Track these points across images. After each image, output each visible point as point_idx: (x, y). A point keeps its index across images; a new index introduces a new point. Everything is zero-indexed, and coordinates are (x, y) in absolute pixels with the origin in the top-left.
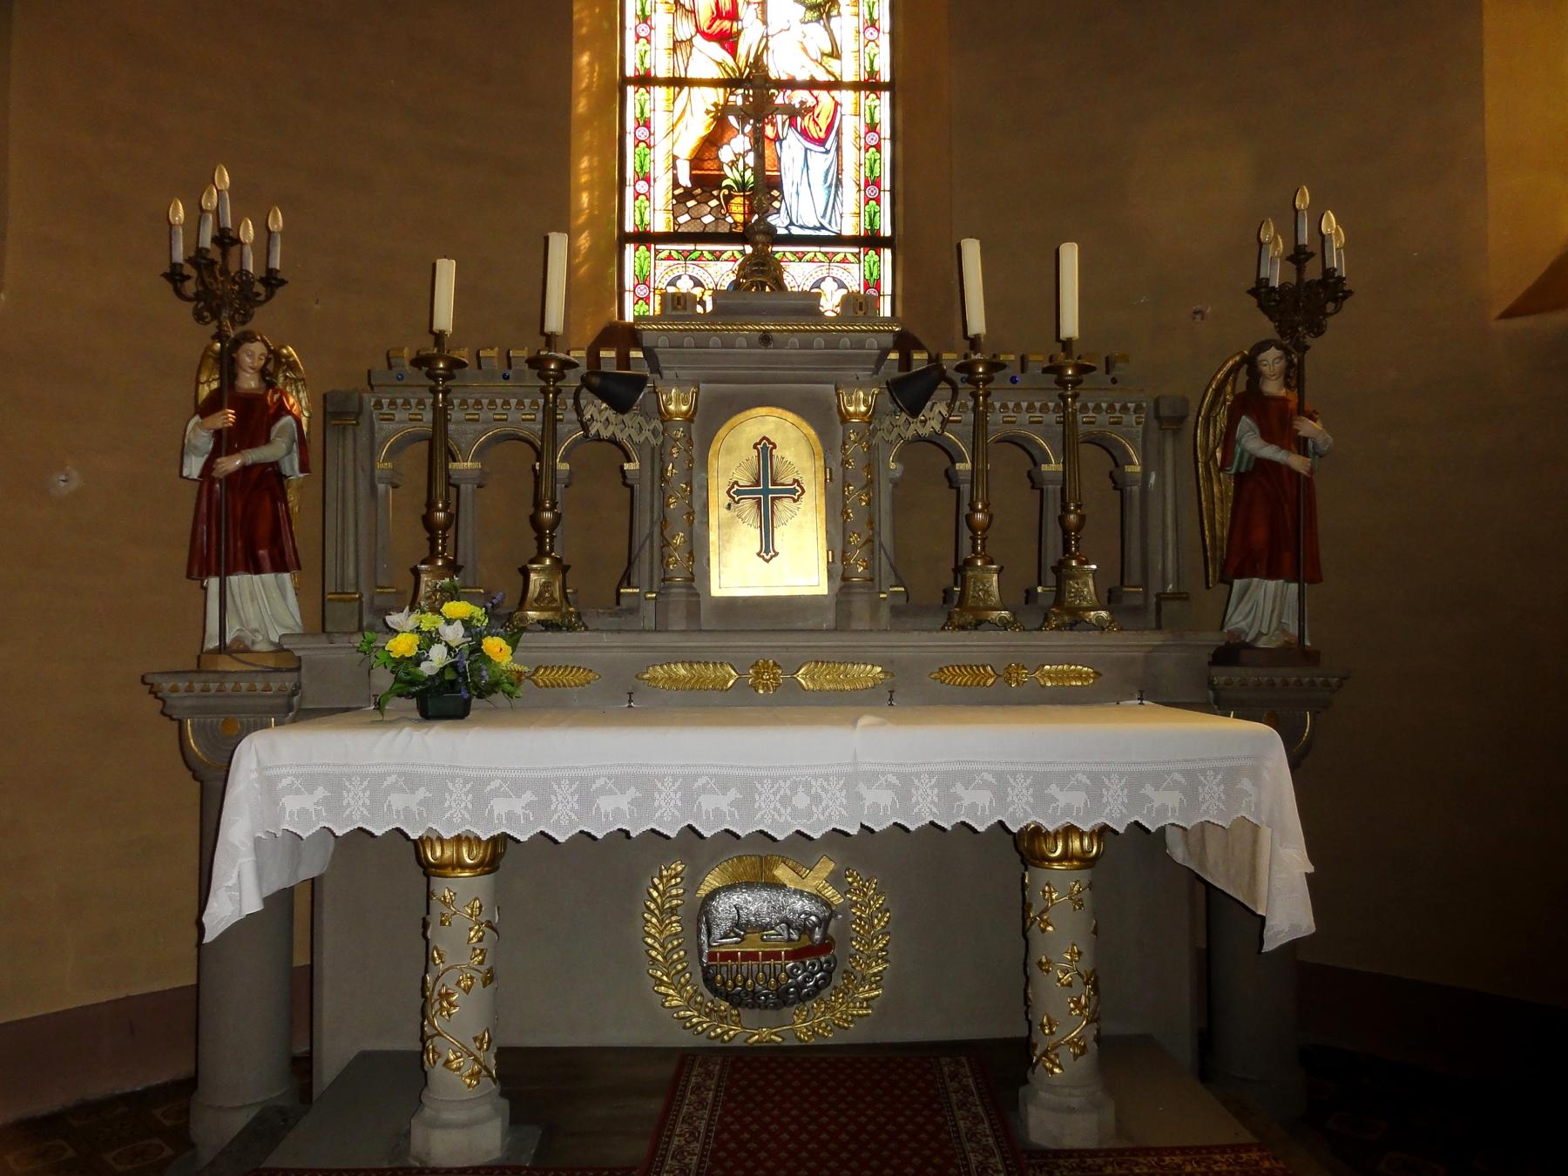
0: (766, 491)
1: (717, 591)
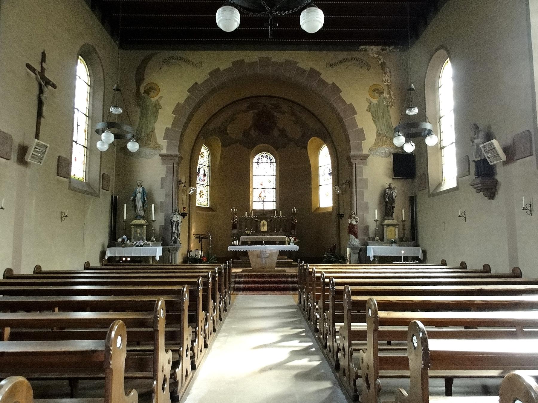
0: (264, 225)
1: (352, 329)
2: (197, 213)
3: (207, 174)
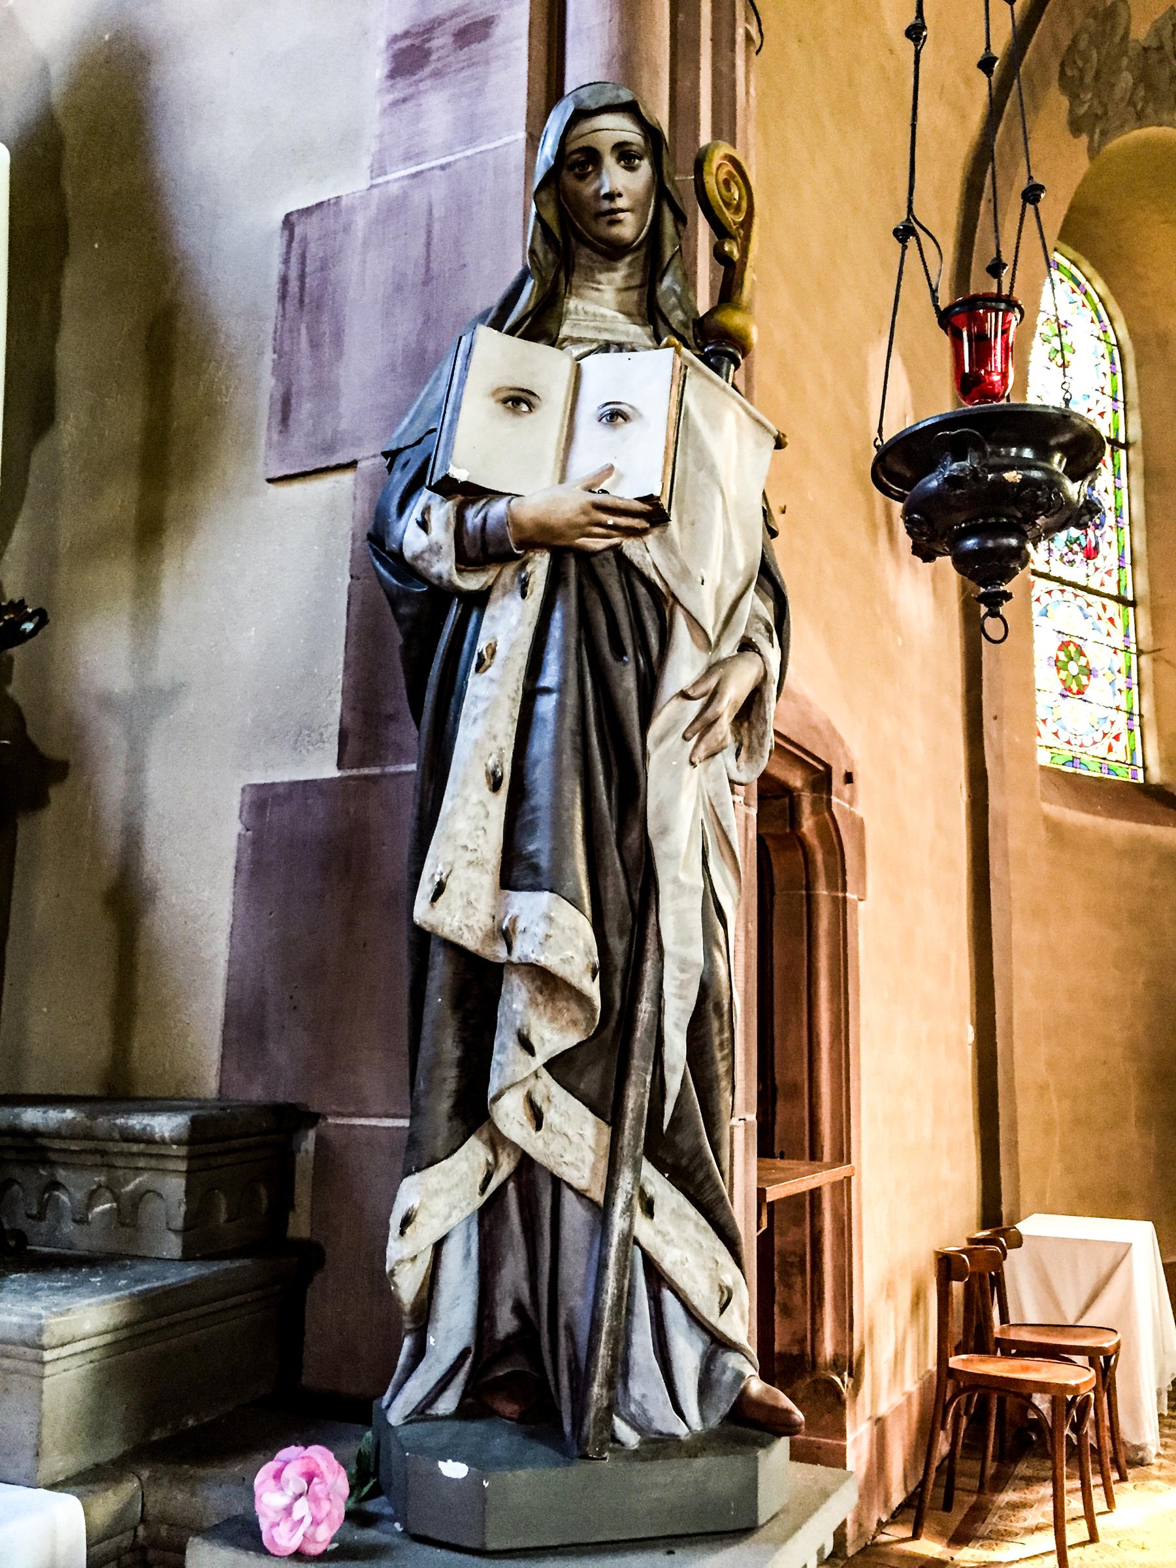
2: (1055, 829)
3: (1107, 502)
